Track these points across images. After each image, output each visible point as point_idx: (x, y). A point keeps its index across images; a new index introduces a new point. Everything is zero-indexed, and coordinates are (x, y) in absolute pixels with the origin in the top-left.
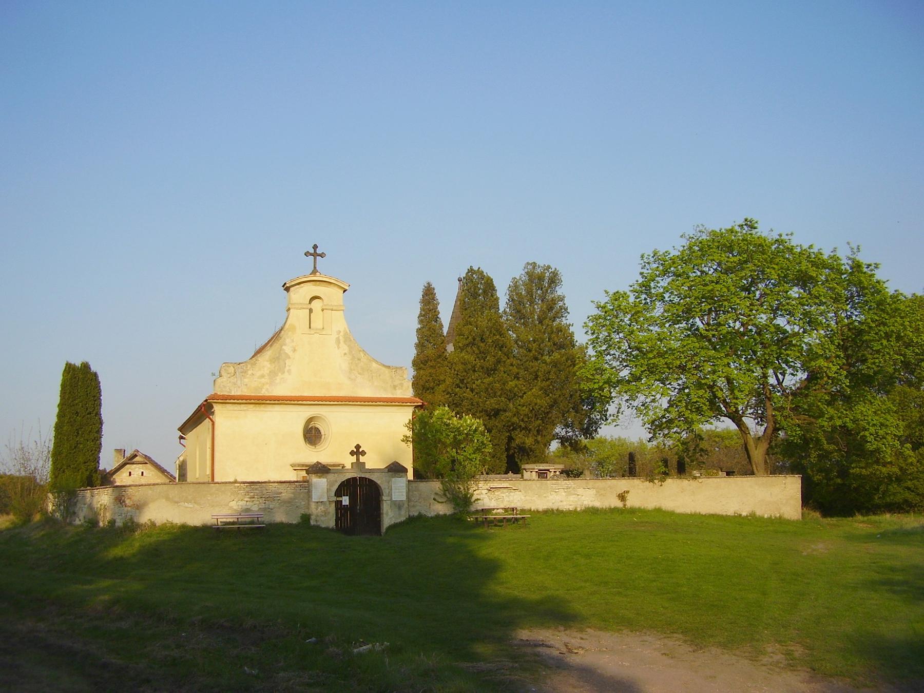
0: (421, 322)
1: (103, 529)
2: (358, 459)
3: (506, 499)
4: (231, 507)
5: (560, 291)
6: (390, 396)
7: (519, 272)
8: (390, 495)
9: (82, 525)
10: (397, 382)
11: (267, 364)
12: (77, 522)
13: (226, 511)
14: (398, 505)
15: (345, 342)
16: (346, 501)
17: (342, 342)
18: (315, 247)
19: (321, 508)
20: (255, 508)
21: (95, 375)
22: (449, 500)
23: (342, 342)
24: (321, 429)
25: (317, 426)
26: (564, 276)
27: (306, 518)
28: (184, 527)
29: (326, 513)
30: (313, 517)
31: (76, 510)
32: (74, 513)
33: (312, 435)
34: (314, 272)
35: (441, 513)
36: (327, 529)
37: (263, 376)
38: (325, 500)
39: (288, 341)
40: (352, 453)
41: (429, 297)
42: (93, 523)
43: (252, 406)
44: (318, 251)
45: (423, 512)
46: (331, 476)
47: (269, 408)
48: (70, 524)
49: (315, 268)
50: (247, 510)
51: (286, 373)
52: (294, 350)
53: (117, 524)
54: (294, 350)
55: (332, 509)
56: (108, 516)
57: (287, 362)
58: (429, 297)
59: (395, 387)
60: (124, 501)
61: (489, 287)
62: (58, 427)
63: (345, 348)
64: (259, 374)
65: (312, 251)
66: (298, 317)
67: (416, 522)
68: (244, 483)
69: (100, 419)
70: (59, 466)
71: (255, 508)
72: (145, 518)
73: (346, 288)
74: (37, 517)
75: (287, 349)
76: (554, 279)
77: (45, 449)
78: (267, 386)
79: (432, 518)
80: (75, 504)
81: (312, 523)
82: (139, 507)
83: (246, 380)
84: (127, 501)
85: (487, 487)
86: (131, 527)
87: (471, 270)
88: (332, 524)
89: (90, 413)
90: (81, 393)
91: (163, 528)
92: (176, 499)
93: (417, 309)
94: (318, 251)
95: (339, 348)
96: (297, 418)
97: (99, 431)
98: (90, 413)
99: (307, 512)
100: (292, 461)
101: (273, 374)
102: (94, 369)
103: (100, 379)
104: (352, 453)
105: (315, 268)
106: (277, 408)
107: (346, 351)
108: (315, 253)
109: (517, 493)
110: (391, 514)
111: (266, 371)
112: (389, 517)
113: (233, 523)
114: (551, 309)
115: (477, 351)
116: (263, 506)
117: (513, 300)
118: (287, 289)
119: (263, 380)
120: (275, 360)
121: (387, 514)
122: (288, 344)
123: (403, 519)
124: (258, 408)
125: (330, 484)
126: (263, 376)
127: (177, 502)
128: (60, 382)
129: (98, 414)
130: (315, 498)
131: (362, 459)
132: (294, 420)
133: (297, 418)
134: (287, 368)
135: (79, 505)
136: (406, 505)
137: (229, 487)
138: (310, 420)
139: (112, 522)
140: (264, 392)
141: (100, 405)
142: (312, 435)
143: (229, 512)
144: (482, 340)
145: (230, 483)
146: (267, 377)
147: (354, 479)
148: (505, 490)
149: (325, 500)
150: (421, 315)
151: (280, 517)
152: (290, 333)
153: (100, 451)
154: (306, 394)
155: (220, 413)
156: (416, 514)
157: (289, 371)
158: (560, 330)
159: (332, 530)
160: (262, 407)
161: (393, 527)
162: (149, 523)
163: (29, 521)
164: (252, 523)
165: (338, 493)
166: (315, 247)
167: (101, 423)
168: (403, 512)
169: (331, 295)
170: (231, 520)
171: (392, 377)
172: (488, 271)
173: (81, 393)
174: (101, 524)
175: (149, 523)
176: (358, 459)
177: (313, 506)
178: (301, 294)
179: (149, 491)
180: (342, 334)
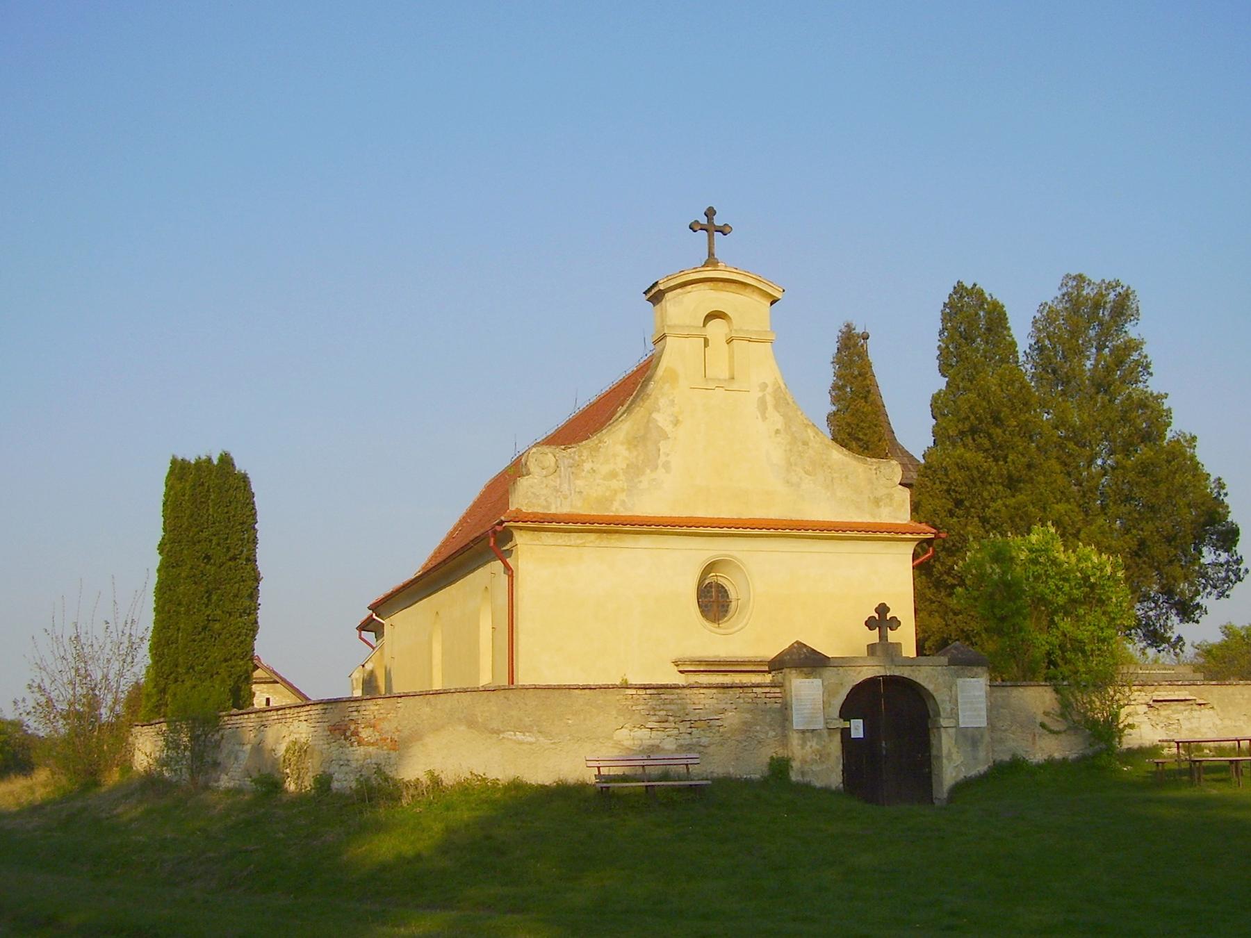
0: (836, 400)
1: (300, 800)
2: (883, 637)
3: (1186, 725)
4: (618, 743)
5: (1133, 331)
6: (866, 518)
7: (1050, 292)
8: (954, 715)
9: (238, 791)
10: (882, 492)
11: (622, 450)
12: (225, 782)
13: (607, 751)
14: (970, 738)
15: (776, 407)
16: (857, 728)
17: (770, 408)
18: (710, 213)
19: (813, 744)
20: (669, 745)
21: (245, 479)
22: (1074, 728)
23: (770, 408)
24: (729, 587)
25: (722, 581)
26: (1144, 301)
27: (780, 768)
28: (516, 786)
29: (822, 756)
30: (796, 765)
31: (221, 757)
32: (216, 764)
33: (714, 600)
34: (711, 261)
35: (1057, 756)
36: (826, 790)
37: (613, 475)
38: (820, 725)
39: (662, 402)
40: (870, 623)
41: (852, 353)
42: (270, 785)
43: (592, 536)
44: (718, 221)
45: (1021, 753)
46: (828, 673)
47: (629, 541)
48: (206, 787)
49: (711, 254)
50: (655, 748)
51: (661, 470)
52: (676, 423)
53: (335, 785)
54: (676, 423)
55: (835, 746)
56: (312, 768)
57: (662, 445)
58: (852, 353)
59: (877, 502)
60: (356, 733)
61: (997, 319)
62: (165, 591)
63: (776, 420)
64: (605, 469)
65: (704, 221)
66: (679, 356)
67: (1009, 772)
68: (645, 688)
69: (255, 569)
70: (166, 669)
71: (669, 745)
72: (414, 769)
73: (778, 295)
74: (113, 777)
75: (662, 419)
76: (1122, 308)
77: (125, 640)
78: (623, 496)
79: (1039, 766)
80: (217, 745)
81: (794, 777)
82: (399, 746)
83: (580, 483)
84: (365, 734)
85: (1147, 699)
86: (378, 792)
87: (960, 290)
88: (834, 778)
89: (234, 558)
90: (210, 520)
91: (464, 789)
92: (495, 725)
93: (827, 375)
94: (718, 221)
95: (764, 418)
96: (682, 563)
97: (253, 595)
98: (234, 558)
99: (781, 752)
100: (677, 655)
101: (634, 471)
102: (241, 465)
103: (254, 488)
104: (870, 623)
105: (711, 254)
106: (645, 541)
107: (779, 426)
108: (710, 226)
109: (1206, 711)
110: (958, 758)
111: (621, 464)
112: (954, 765)
113: (624, 778)
114: (1120, 363)
115: (987, 444)
116: (686, 740)
117: (1041, 349)
118: (655, 296)
119: (614, 484)
120: (635, 441)
121: (950, 754)
122: (668, 401)
123: (982, 768)
124: (606, 540)
125: (829, 692)
126: (613, 475)
127: (498, 732)
128: (161, 498)
129: (251, 560)
130: (798, 722)
131: (892, 636)
132: (678, 565)
133: (682, 563)
134: (663, 458)
135: (226, 747)
136: (987, 738)
137: (613, 696)
138: (710, 567)
139: (324, 782)
140: (617, 509)
141: (255, 541)
142: (714, 600)
143: (615, 753)
144: (997, 420)
145: (614, 687)
146: (622, 477)
147: (871, 683)
148: (1180, 706)
149: (820, 725)
150: (835, 387)
151: (718, 763)
152: (667, 386)
153: (253, 637)
154: (701, 513)
155: (529, 552)
156: (1007, 758)
157: (667, 466)
158: (1143, 404)
159: (836, 793)
160: (614, 540)
161: (963, 787)
162: (425, 779)
163: (97, 784)
164: (665, 777)
165: (847, 712)
166: (710, 213)
167: (257, 579)
168: (982, 754)
169: (748, 310)
170: (627, 771)
171: (870, 482)
172: (993, 290)
173: (210, 520)
174: (291, 786)
175: (425, 779)
176: (883, 637)
177: (795, 740)
178: (685, 307)
179: (424, 709)
180: (770, 389)
